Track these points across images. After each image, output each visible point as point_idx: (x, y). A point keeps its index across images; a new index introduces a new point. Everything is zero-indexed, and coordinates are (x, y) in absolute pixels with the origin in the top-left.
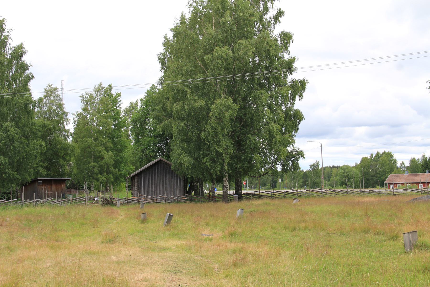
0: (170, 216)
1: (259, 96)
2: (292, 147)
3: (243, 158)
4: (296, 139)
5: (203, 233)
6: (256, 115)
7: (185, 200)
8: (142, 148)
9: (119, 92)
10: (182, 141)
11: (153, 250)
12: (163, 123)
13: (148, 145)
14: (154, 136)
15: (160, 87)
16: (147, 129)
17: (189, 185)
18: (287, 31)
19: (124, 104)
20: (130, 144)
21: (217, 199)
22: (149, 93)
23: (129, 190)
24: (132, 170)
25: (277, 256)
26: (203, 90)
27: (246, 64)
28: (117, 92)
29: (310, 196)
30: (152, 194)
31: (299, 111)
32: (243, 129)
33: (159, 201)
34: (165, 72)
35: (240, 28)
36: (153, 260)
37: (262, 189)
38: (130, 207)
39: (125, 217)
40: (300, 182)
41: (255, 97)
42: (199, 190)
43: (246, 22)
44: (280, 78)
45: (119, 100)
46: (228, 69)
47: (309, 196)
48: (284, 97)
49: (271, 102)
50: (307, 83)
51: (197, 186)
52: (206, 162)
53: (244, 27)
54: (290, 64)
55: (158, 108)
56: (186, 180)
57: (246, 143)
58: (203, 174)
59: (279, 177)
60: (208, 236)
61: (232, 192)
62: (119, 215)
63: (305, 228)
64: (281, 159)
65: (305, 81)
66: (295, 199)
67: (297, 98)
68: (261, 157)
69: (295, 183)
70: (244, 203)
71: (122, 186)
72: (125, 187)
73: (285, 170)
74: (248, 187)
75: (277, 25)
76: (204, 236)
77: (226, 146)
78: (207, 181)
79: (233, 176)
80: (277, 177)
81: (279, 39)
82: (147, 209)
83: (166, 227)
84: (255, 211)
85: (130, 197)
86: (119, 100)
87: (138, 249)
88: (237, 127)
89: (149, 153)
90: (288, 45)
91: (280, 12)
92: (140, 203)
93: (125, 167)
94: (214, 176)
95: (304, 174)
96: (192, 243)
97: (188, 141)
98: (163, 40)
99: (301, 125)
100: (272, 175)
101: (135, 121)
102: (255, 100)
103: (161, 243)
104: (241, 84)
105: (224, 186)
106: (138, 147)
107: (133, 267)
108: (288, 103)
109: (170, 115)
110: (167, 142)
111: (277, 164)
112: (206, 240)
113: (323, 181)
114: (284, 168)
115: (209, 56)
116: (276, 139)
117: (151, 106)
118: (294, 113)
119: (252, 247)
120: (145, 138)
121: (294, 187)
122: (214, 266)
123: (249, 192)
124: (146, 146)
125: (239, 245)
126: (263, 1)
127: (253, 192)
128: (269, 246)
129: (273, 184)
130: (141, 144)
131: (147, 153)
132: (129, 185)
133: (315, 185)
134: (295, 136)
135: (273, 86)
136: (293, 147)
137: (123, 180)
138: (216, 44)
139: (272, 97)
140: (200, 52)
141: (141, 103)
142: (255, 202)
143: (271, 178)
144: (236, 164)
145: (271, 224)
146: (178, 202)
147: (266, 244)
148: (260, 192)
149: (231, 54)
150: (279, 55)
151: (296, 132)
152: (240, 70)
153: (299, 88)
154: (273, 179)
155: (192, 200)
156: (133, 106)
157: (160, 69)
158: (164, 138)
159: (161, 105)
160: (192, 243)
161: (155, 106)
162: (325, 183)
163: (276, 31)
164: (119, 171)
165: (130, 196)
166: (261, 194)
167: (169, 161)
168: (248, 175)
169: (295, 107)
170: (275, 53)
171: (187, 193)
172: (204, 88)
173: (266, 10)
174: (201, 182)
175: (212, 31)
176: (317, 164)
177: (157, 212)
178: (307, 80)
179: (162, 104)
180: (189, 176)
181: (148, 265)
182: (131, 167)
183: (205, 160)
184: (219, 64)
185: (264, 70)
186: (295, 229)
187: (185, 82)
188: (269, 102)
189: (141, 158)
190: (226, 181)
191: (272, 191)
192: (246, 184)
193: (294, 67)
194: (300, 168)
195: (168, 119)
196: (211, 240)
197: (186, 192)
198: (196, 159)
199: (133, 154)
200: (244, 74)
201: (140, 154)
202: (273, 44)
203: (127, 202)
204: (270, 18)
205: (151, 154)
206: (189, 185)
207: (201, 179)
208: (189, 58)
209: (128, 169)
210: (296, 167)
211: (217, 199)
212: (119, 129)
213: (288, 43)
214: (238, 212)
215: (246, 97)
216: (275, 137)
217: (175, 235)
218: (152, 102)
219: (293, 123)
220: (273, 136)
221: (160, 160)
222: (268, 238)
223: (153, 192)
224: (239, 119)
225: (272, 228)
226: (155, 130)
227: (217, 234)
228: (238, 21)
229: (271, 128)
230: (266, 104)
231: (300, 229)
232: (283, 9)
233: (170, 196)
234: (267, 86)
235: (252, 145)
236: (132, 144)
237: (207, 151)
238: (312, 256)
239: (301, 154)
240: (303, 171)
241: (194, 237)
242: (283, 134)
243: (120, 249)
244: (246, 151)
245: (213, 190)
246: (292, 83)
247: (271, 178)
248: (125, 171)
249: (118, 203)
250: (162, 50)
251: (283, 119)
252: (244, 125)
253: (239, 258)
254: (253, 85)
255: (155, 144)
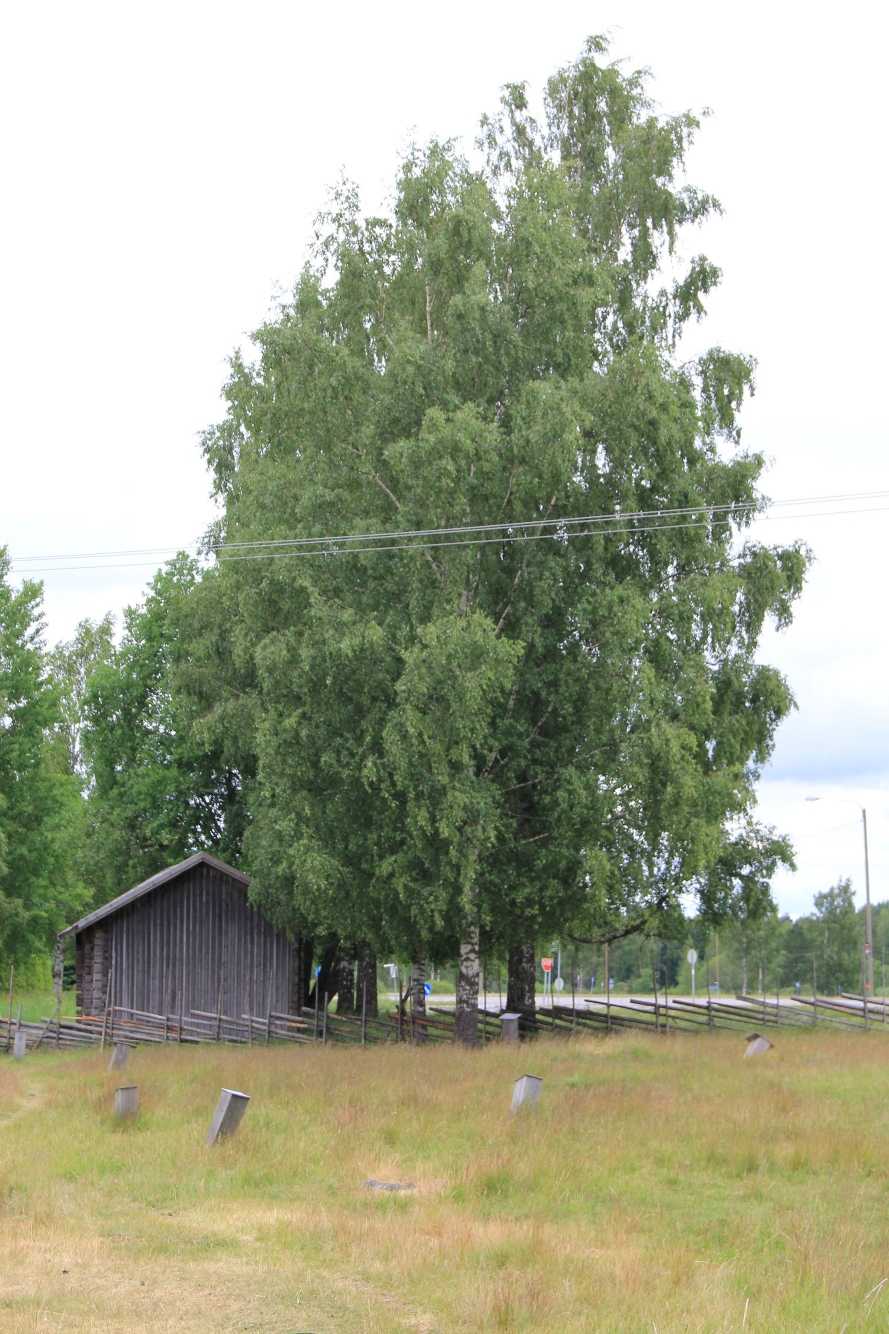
0: (238, 1102)
1: (610, 608)
2: (743, 822)
3: (540, 864)
4: (758, 787)
5: (371, 1177)
6: (598, 688)
7: (299, 1030)
8: (129, 813)
9: (36, 581)
10: (297, 785)
11: (162, 1249)
12: (218, 709)
13: (154, 799)
14: (180, 763)
15: (208, 562)
16: (148, 732)
17: (316, 970)
18: (732, 347)
19: (55, 629)
20: (76, 794)
21: (431, 1030)
22: (167, 586)
23: (68, 985)
24: (79, 901)
25: (677, 1283)
26: (375, 584)
27: (556, 478)
28: (27, 579)
29: (814, 1024)
30: (161, 1004)
31: (777, 673)
32: (546, 745)
33: (192, 1033)
34: (232, 500)
35: (539, 333)
36: (158, 1294)
37: (618, 991)
38: (68, 1057)
39: (49, 1104)
40: (773, 965)
41: (594, 611)
42: (360, 990)
43: (561, 307)
44: (698, 538)
45: (36, 612)
46: (486, 498)
47: (812, 1027)
48: (715, 616)
49: (661, 634)
50: (810, 559)
51: (351, 973)
52: (392, 875)
53: (549, 330)
54: (741, 483)
55: (199, 647)
56: (304, 952)
57: (556, 803)
58: (375, 923)
59: (690, 941)
60: (392, 1188)
61: (493, 1001)
62: (22, 1095)
63: (796, 1165)
64: (694, 872)
65: (803, 552)
66: (756, 1037)
67: (769, 620)
68: (614, 859)
69: (753, 969)
70: (544, 1050)
71: (39, 969)
72: (49, 973)
73: (715, 914)
74: (559, 983)
75: (690, 324)
76: (377, 1190)
77: (471, 809)
78: (391, 952)
79: (501, 935)
80: (682, 942)
81: (698, 381)
82: (142, 1067)
83: (218, 1149)
84: (587, 1086)
85: (71, 1018)
86: (36, 612)
87: (96, 1242)
88: (520, 735)
89: (155, 832)
90: (734, 404)
91: (703, 271)
92: (110, 1044)
93: (51, 892)
94: (425, 935)
95: (792, 931)
96: (326, 1220)
97: (319, 786)
98: (225, 375)
99: (785, 733)
100: (659, 935)
101: (99, 701)
102: (595, 624)
103: (196, 1220)
104: (540, 557)
105: (462, 977)
106: (112, 808)
107: (72, 1325)
108: (728, 642)
109: (248, 680)
110: (232, 791)
111: (680, 891)
112: (382, 1207)
113: (870, 963)
114: (710, 907)
115: (402, 445)
116: (679, 786)
117: (170, 639)
118: (755, 684)
119: (573, 1240)
120: (141, 770)
121: (752, 987)
122: (413, 1321)
123: (565, 1001)
124: (142, 805)
125: (523, 1232)
126: (632, 226)
127: (580, 1002)
128: (643, 1238)
129: (662, 973)
130: (121, 795)
131: (148, 833)
132: (68, 963)
133: (838, 977)
134: (757, 777)
135: (671, 570)
136: (749, 823)
137: (38, 944)
138: (430, 395)
139: (663, 612)
140: (368, 431)
141: (129, 628)
142: (590, 1047)
143: (654, 945)
144: (513, 888)
145: (654, 1144)
146: (269, 1038)
147: (634, 1228)
148: (609, 1005)
149: (493, 434)
150: (698, 443)
151: (761, 758)
152: (530, 503)
153: (775, 579)
154: (665, 948)
155: (327, 1033)
156: (93, 639)
157: (211, 489)
158: (219, 770)
159: (211, 637)
160: (326, 1220)
161: (187, 637)
162: (877, 973)
163: (685, 349)
164: (27, 906)
165: (70, 1014)
166: (614, 1011)
167: (236, 867)
168: (561, 933)
169: (760, 658)
170: (678, 435)
171: (310, 1002)
172: (389, 570)
173: (645, 259)
174: (368, 956)
175: (416, 348)
176: (845, 891)
177: (185, 1079)
178: (809, 551)
179: (216, 631)
180: (321, 931)
181: (138, 1315)
182: (80, 889)
183: (385, 867)
184: (448, 474)
185: (632, 503)
186: (751, 1167)
187: (312, 548)
188: (652, 634)
189: (122, 852)
190: (472, 956)
191: (661, 1001)
192: (554, 968)
193: (756, 495)
194: (774, 909)
195: (237, 697)
196: (403, 1206)
197: (306, 999)
198: (349, 860)
199: (89, 835)
200: (552, 522)
201: (117, 834)
202: (673, 398)
203: (55, 1037)
204: (663, 293)
205: (166, 837)
206: (316, 970)
207: (368, 945)
208: (329, 449)
209: (65, 897)
210: (759, 902)
211: (431, 1030)
212: (30, 732)
213: (735, 396)
214: (520, 1090)
215: (559, 613)
216: (674, 781)
217: (257, 1186)
218: (175, 622)
219: (749, 724)
220: (665, 774)
221: (202, 865)
222: (643, 1202)
223: (167, 998)
224: (531, 704)
225: (660, 1161)
226: (182, 739)
227: (428, 1181)
228: (523, 301)
229: (657, 743)
230: (638, 642)
231: (772, 1168)
232: (714, 260)
233: (238, 1016)
234: (645, 568)
235: (578, 809)
236: (85, 795)
237: (395, 829)
238: (824, 1291)
239: (780, 851)
240: (787, 919)
241: (333, 1192)
242: (707, 767)
243: (22, 1243)
244: (555, 834)
245: (418, 991)
246: (749, 559)
247: (654, 945)
248: (52, 905)
249: (19, 1044)
250: (220, 411)
251: (709, 706)
252: (544, 728)
253: (521, 1291)
254: (588, 564)
255: (182, 795)
